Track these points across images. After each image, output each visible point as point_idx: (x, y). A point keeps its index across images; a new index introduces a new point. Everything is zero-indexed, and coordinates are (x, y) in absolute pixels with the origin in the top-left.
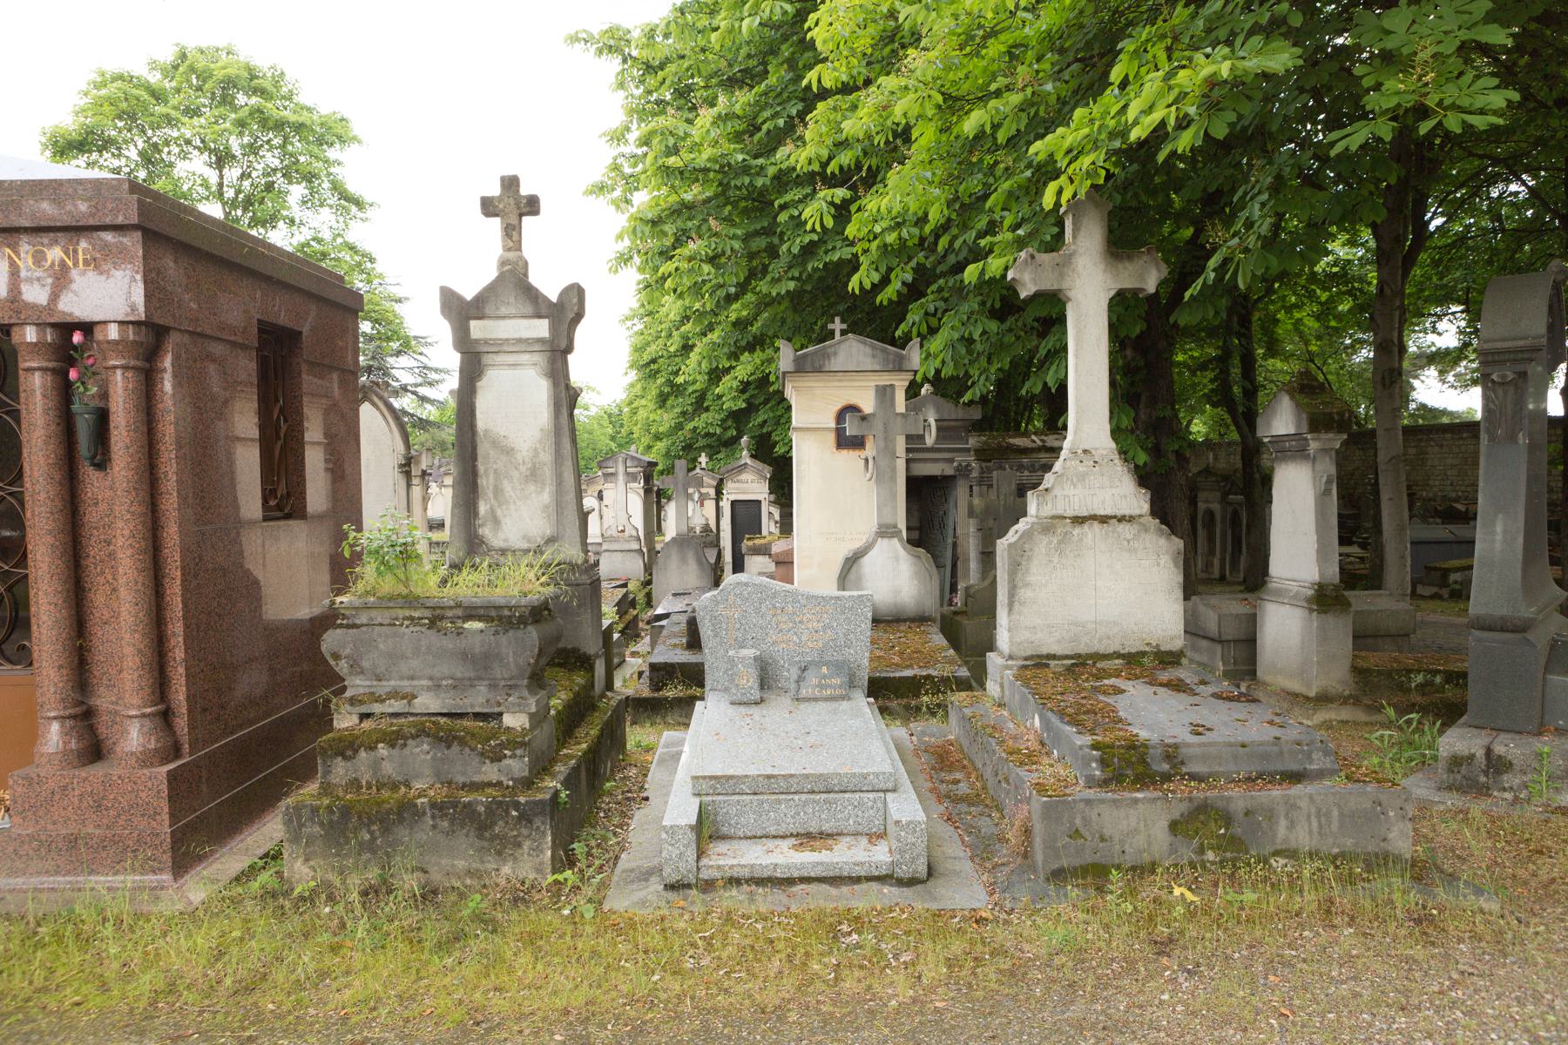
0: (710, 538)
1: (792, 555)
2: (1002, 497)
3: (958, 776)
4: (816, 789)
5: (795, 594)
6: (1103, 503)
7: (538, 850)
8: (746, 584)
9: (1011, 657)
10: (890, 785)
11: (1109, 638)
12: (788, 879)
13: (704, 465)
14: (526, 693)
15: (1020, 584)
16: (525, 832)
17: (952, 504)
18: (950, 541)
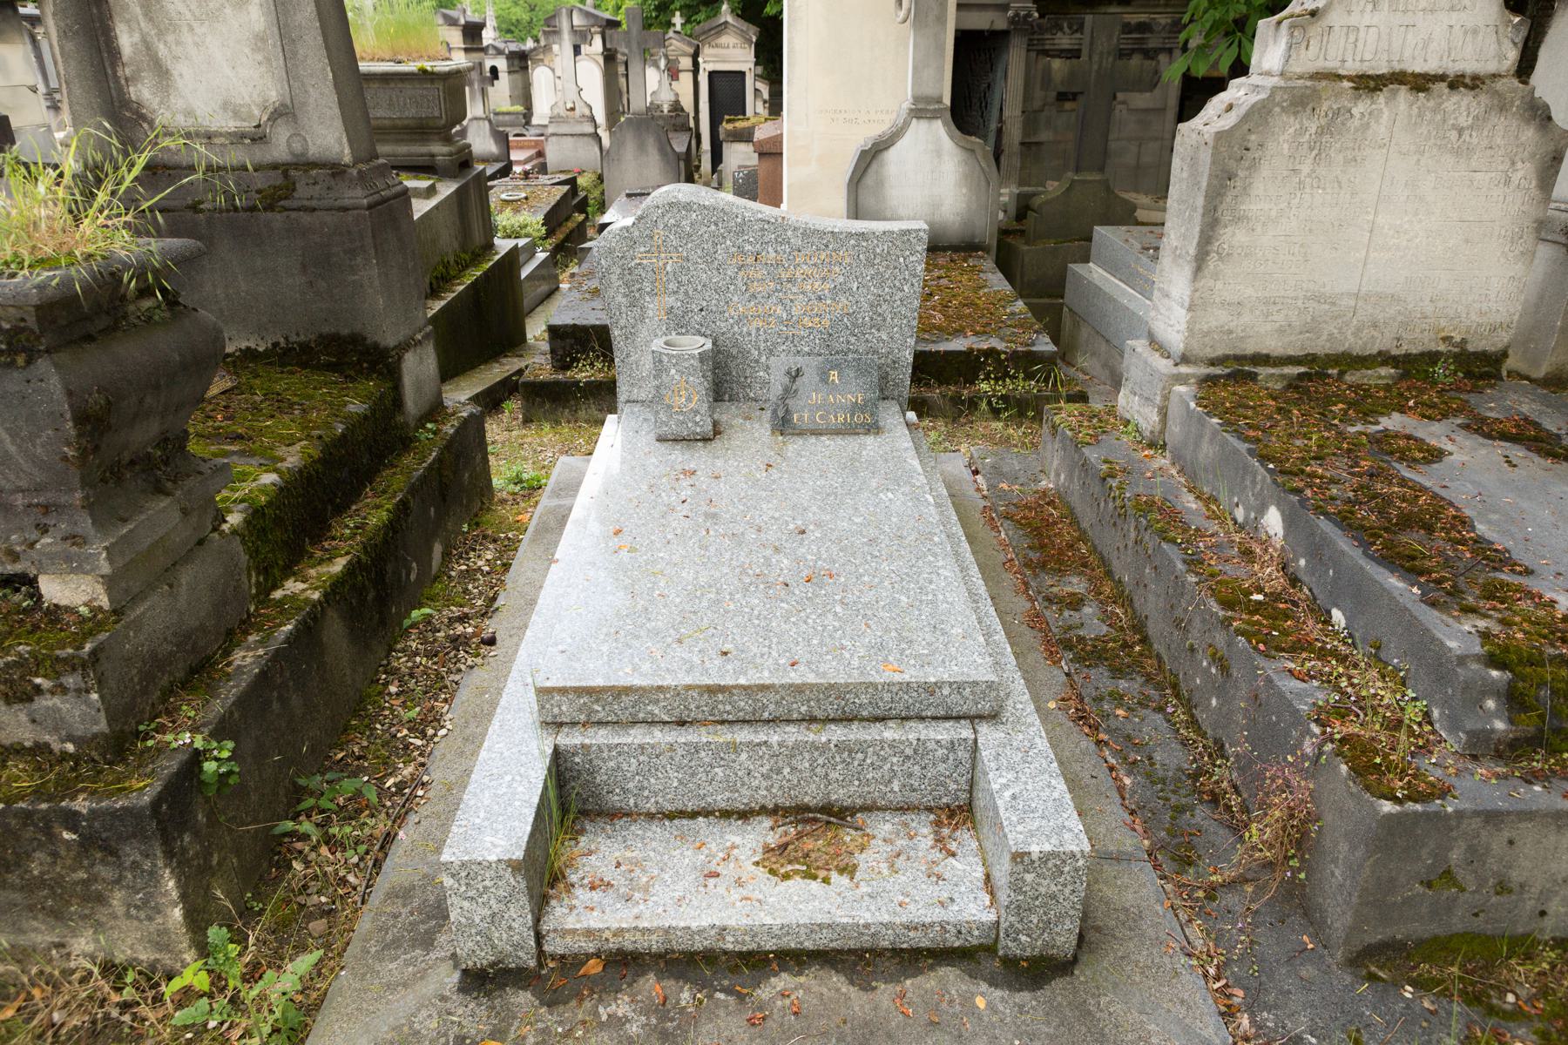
0: (677, 119)
1: (781, 143)
2: (1096, 58)
3: (1076, 584)
4: (819, 714)
5: (781, 226)
6: (1425, 46)
7: (150, 907)
8: (688, 207)
9: (1185, 359)
10: (985, 707)
11: (1375, 326)
12: (750, 953)
13: (678, 28)
14: (85, 524)
15: (1226, 218)
16: (106, 872)
17: (1000, 74)
18: (993, 126)
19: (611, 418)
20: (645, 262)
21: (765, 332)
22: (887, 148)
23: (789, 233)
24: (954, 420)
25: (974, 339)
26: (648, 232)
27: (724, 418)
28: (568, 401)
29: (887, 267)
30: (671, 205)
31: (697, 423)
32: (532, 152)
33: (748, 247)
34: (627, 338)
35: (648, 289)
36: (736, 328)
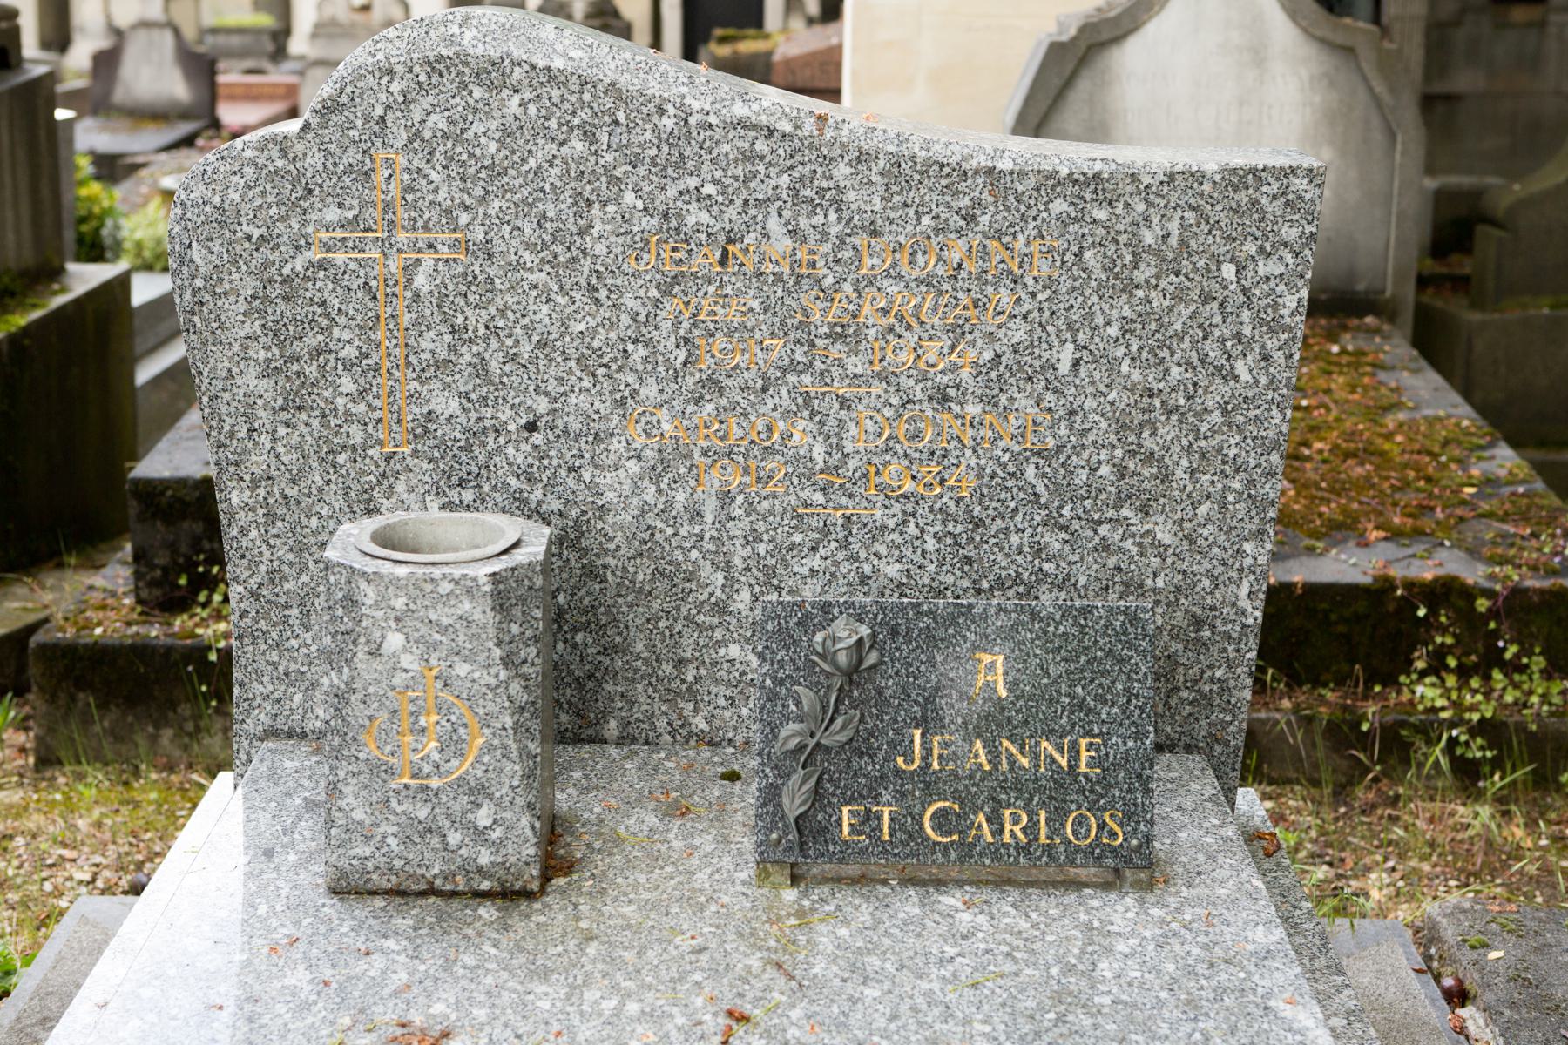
8: (493, 74)
19: (225, 778)
20: (340, 258)
21: (750, 509)
22: (1118, 39)
23: (842, 171)
24: (1341, 792)
25: (1390, 550)
26: (352, 156)
27: (593, 807)
28: (173, 705)
29: (1180, 296)
30: (435, 65)
31: (480, 834)
32: (279, 107)
33: (696, 216)
34: (271, 517)
35: (350, 352)
36: (650, 494)
